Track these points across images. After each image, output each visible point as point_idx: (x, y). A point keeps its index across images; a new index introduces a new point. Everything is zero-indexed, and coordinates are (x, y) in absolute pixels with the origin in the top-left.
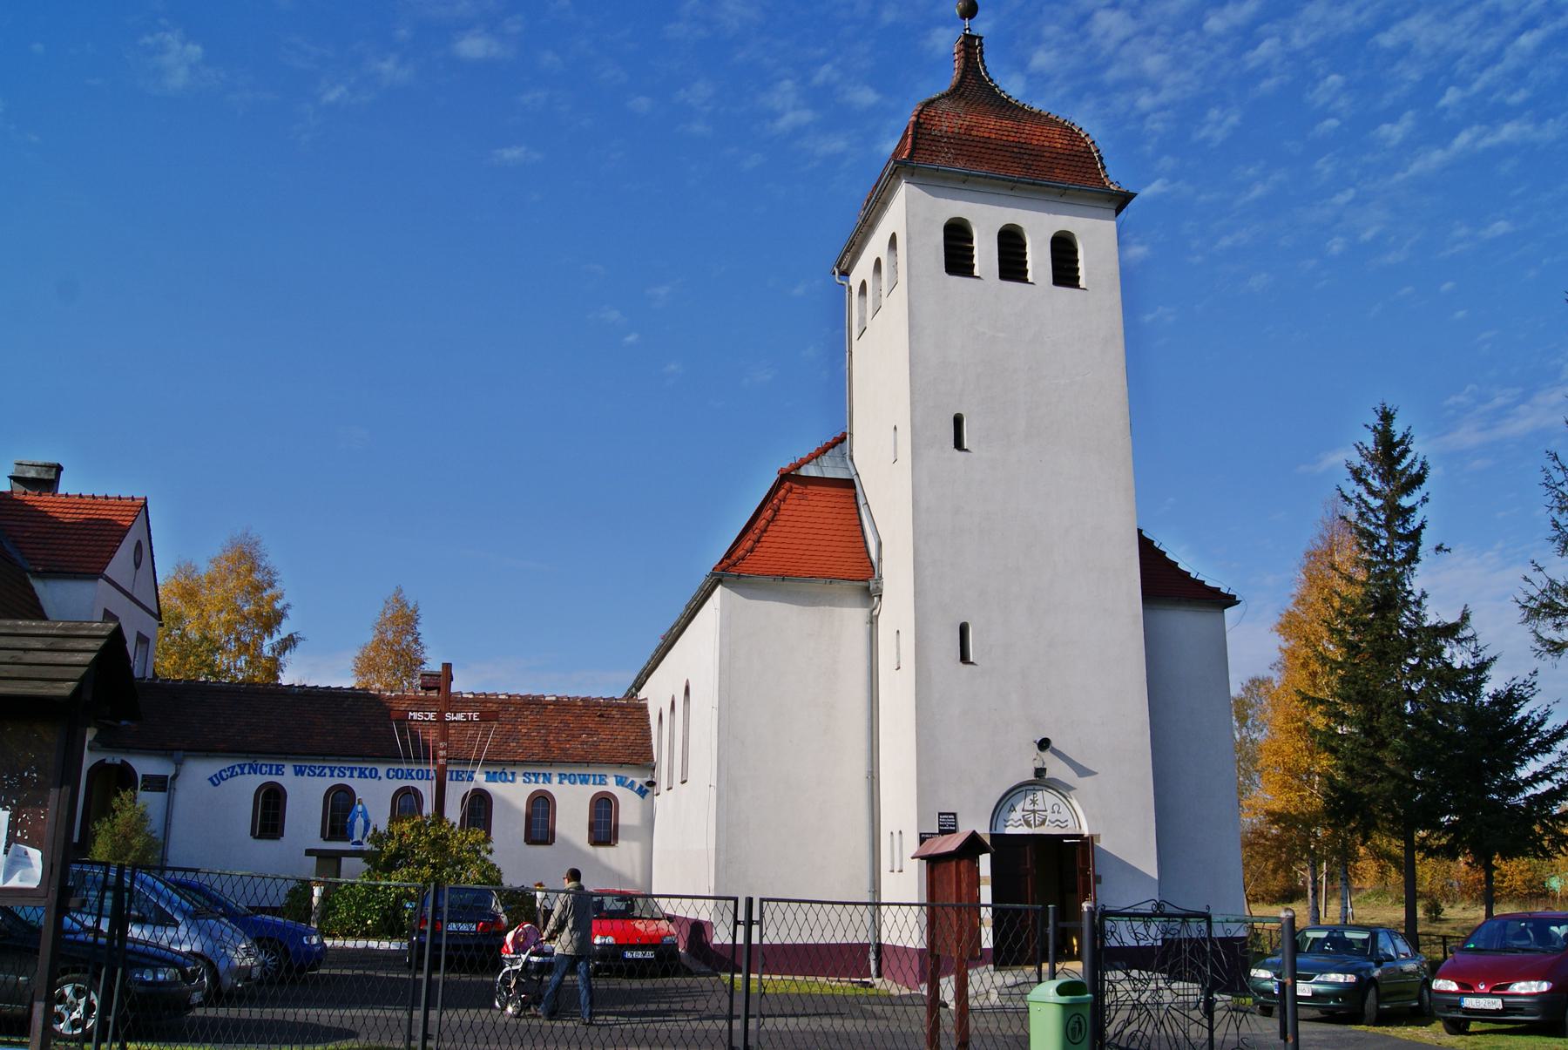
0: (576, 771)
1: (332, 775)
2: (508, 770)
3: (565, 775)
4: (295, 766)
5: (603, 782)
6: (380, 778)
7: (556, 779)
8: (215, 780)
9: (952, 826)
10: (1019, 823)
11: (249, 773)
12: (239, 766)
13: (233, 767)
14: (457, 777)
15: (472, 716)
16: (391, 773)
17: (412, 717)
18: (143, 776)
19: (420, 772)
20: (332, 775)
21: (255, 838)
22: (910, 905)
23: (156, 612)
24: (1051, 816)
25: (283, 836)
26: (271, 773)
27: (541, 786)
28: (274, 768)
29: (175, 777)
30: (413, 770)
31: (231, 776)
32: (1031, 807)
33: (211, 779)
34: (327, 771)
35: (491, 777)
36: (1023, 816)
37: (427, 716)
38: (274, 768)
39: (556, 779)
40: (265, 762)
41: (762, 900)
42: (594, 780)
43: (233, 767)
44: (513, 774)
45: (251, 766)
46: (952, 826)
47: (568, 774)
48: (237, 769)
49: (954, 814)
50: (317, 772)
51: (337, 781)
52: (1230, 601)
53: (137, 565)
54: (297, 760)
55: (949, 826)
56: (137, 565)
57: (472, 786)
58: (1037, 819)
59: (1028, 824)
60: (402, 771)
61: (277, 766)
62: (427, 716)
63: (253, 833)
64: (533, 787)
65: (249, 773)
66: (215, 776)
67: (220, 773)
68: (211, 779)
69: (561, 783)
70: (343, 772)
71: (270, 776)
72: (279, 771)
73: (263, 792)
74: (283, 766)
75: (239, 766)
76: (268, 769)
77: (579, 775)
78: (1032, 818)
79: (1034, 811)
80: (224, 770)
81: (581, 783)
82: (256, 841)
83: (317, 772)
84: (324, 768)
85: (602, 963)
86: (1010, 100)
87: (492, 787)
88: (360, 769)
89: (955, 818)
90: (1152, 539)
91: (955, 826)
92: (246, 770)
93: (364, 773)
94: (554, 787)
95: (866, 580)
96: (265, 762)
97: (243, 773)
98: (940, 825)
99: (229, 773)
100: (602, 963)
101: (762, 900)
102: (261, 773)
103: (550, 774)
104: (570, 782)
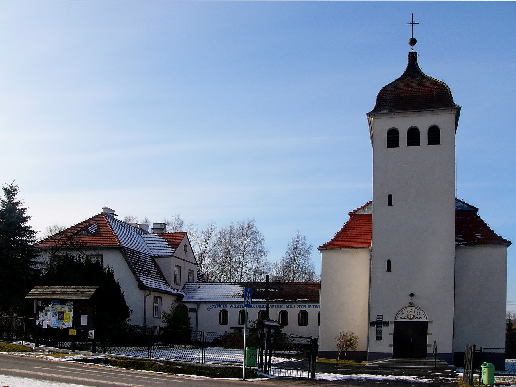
0: (314, 304)
1: (241, 307)
2: (293, 305)
3: (311, 305)
4: (230, 305)
5: (281, 307)
6: (254, 308)
7: (307, 306)
8: (209, 309)
9: (381, 319)
10: (405, 318)
11: (218, 307)
12: (215, 305)
13: (213, 306)
14: (225, 306)
15: (276, 290)
16: (258, 306)
17: (258, 291)
18: (190, 308)
19: (313, 306)
20: (301, 308)
21: (240, 325)
22: (503, 349)
23: (196, 263)
24: (416, 316)
25: (228, 324)
26: (223, 307)
27: (303, 309)
28: (224, 305)
29: (198, 309)
30: (264, 305)
31: (213, 308)
32: (410, 313)
33: (207, 309)
34: (239, 306)
35: (287, 307)
36: (407, 316)
37: (262, 290)
38: (224, 305)
39: (307, 306)
40: (222, 304)
41: (484, 349)
42: (223, 306)
43: (213, 306)
44: (294, 305)
45: (218, 305)
46: (381, 319)
47: (311, 305)
48: (214, 306)
49: (382, 316)
50: (236, 306)
51: (223, 308)
52: (508, 243)
53: (186, 251)
54: (230, 303)
55: (380, 319)
56: (186, 251)
57: (282, 309)
58: (412, 316)
59: (409, 318)
60: (261, 305)
61: (225, 305)
62: (262, 290)
63: (299, 324)
64: (300, 309)
65: (218, 307)
66: (209, 308)
67: (261, 307)
68: (207, 309)
69: (309, 308)
70: (299, 307)
71: (262, 308)
72: (305, 307)
73: (260, 313)
74: (227, 305)
75: (215, 305)
76: (223, 306)
77: (315, 305)
78: (410, 317)
79: (411, 315)
80: (211, 306)
81: (316, 308)
82: (221, 325)
83: (236, 306)
84: (238, 305)
85: (51, 340)
86: (439, 81)
87: (287, 309)
88: (280, 305)
89: (382, 317)
90: (486, 223)
91: (382, 319)
92: (217, 306)
93: (263, 306)
94: (307, 309)
95: (368, 247)
96: (222, 304)
97: (216, 307)
98: (377, 319)
99: (212, 307)
100: (51, 340)
101: (484, 349)
102: (221, 307)
103: (306, 305)
104: (312, 308)
